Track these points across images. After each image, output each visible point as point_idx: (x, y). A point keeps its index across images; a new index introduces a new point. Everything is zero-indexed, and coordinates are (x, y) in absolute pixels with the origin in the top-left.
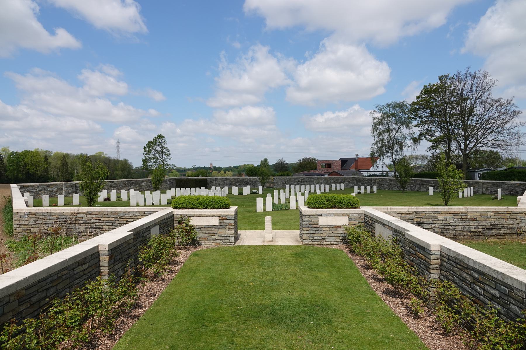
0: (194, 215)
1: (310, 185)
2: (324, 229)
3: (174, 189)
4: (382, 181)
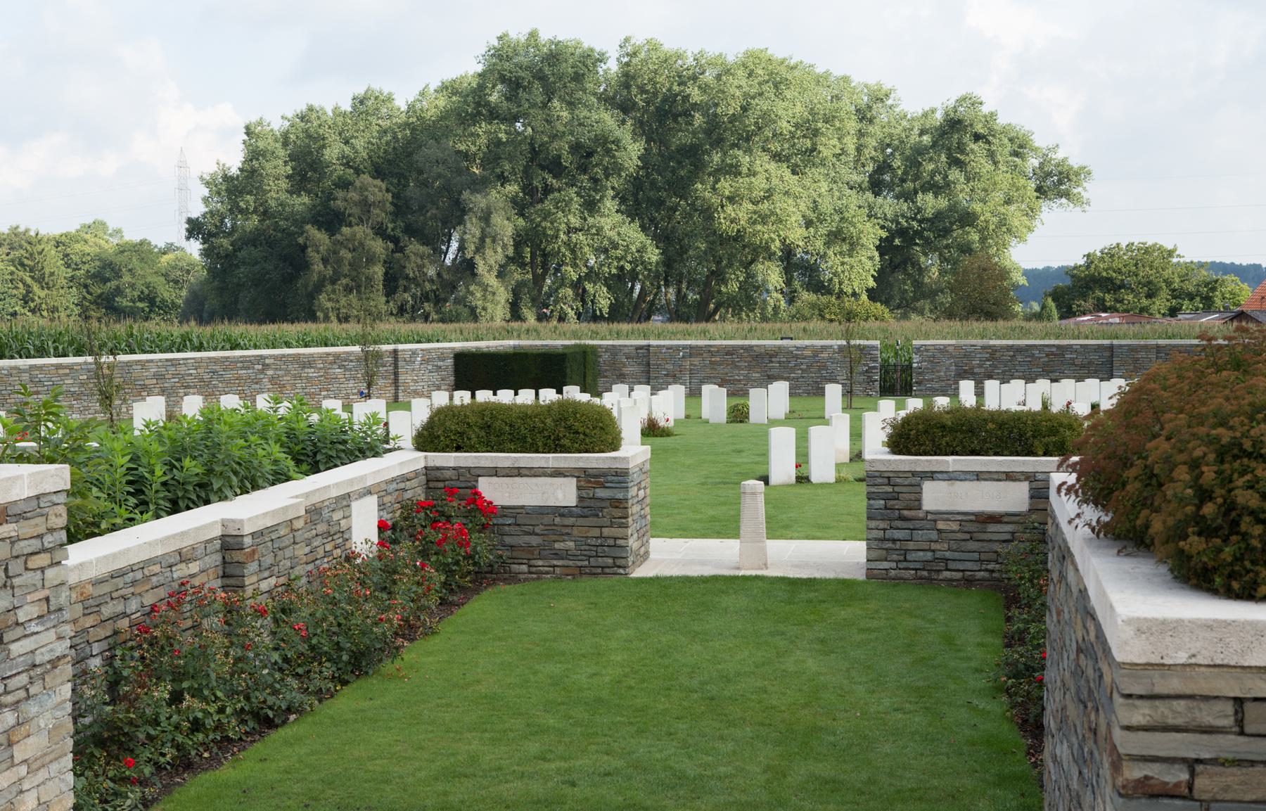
0: (495, 472)
2: (941, 525)
3: (447, 394)
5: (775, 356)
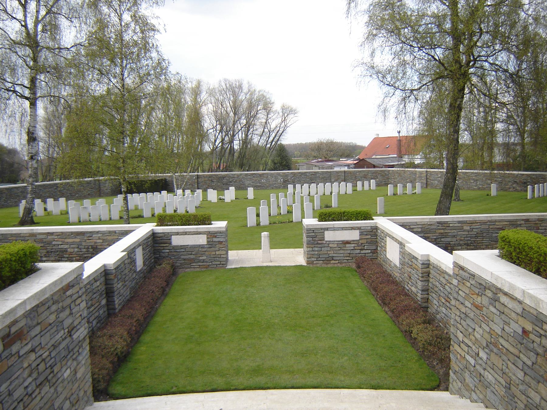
0: (177, 234)
1: (332, 183)
4: (431, 175)
5: (225, 177)
